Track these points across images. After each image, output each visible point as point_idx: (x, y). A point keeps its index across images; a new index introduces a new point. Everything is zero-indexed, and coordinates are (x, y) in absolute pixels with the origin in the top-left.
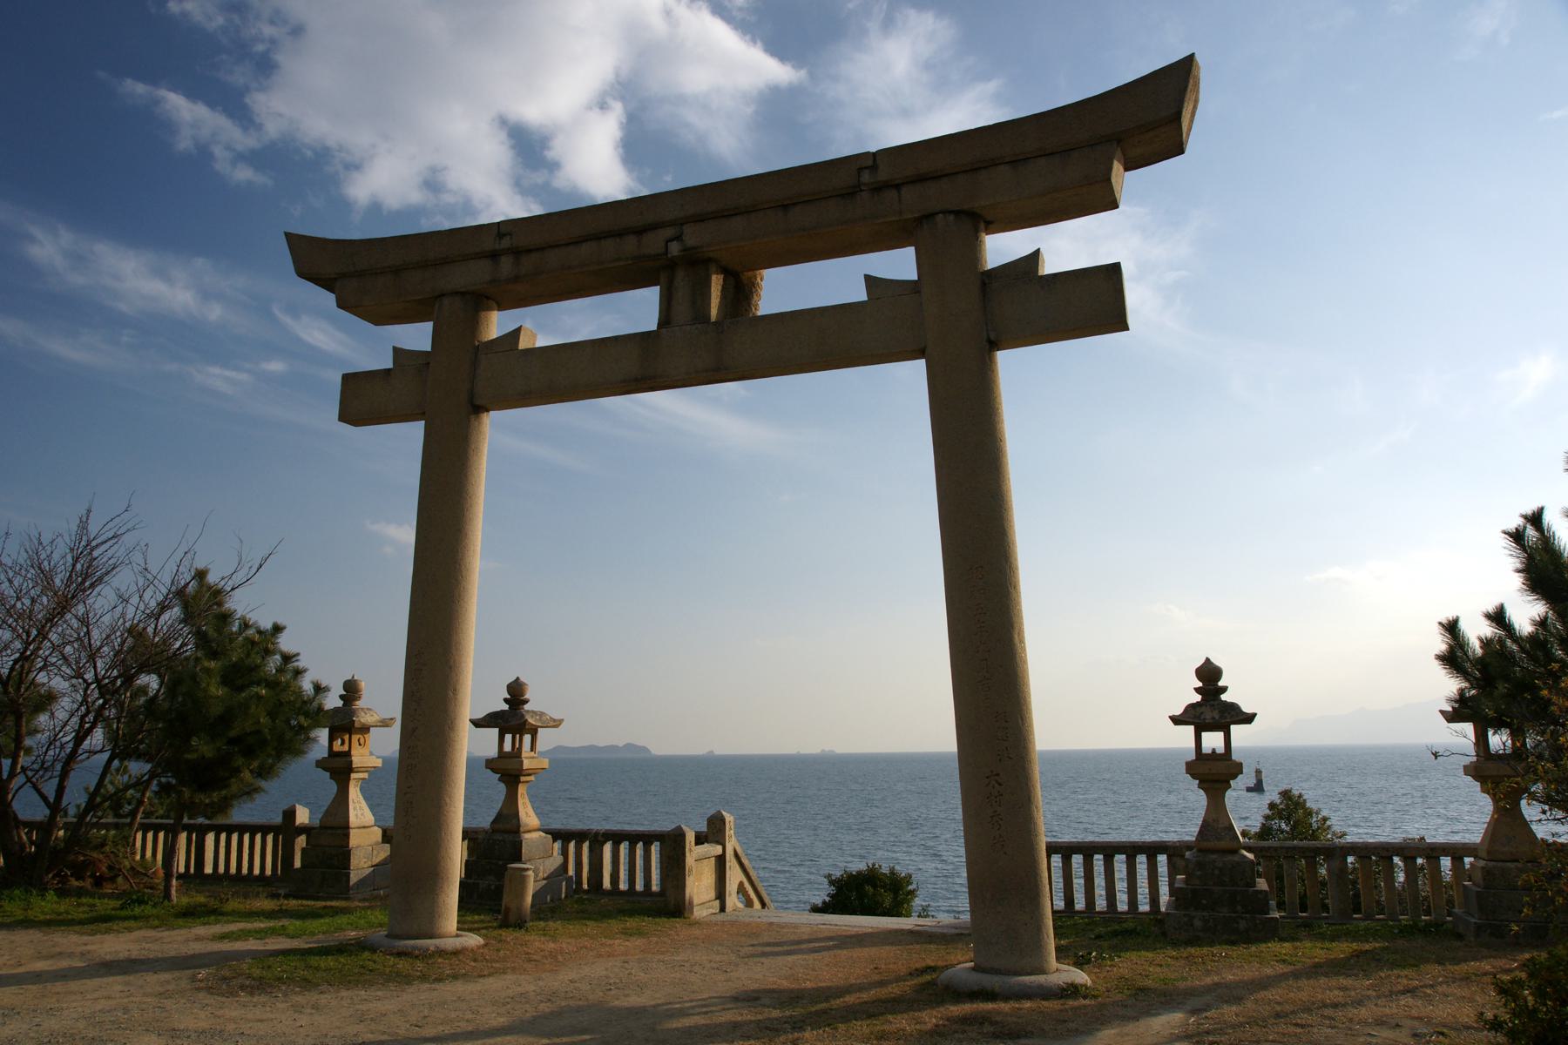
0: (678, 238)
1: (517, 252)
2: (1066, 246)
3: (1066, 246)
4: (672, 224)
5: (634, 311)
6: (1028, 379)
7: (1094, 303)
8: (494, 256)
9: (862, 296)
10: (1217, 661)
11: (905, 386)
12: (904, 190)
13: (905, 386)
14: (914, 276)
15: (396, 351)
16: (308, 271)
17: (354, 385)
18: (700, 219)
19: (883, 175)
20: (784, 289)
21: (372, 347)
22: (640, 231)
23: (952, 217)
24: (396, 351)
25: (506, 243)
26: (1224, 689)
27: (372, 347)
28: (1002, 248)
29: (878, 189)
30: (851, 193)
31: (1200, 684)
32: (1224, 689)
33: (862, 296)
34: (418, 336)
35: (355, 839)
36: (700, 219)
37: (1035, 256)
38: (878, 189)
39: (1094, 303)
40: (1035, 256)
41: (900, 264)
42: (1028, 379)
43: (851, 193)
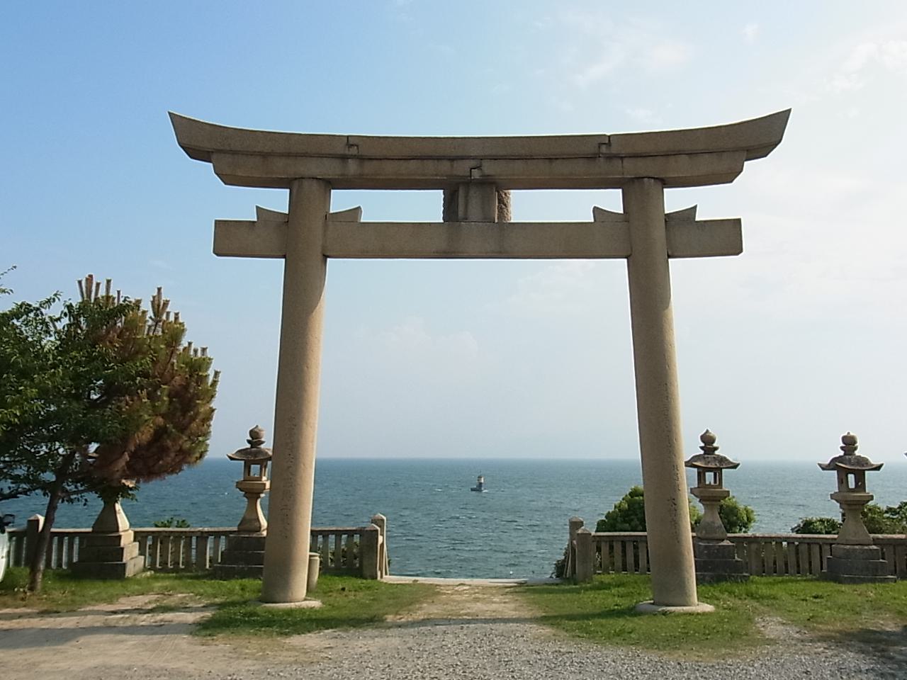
0: (479, 167)
1: (361, 159)
2: (709, 202)
3: (709, 202)
4: (474, 158)
5: (425, 206)
6: (687, 276)
7: (724, 238)
8: (344, 158)
9: (590, 219)
10: (712, 433)
11: (613, 274)
12: (625, 161)
13: (613, 274)
14: (287, 212)
15: (596, 210)
16: (195, 152)
17: (223, 228)
18: (495, 158)
19: (614, 149)
20: (528, 206)
21: (246, 203)
22: (452, 159)
23: (653, 180)
24: (596, 210)
25: (354, 151)
26: (716, 449)
27: (246, 203)
28: (675, 200)
29: (610, 157)
30: (592, 158)
31: (703, 445)
32: (716, 449)
33: (590, 219)
34: (278, 200)
35: (126, 557)
36: (495, 158)
37: (357, 210)
38: (610, 157)
39: (724, 238)
40: (357, 210)
41: (612, 200)
42: (687, 276)
43: (592, 158)
